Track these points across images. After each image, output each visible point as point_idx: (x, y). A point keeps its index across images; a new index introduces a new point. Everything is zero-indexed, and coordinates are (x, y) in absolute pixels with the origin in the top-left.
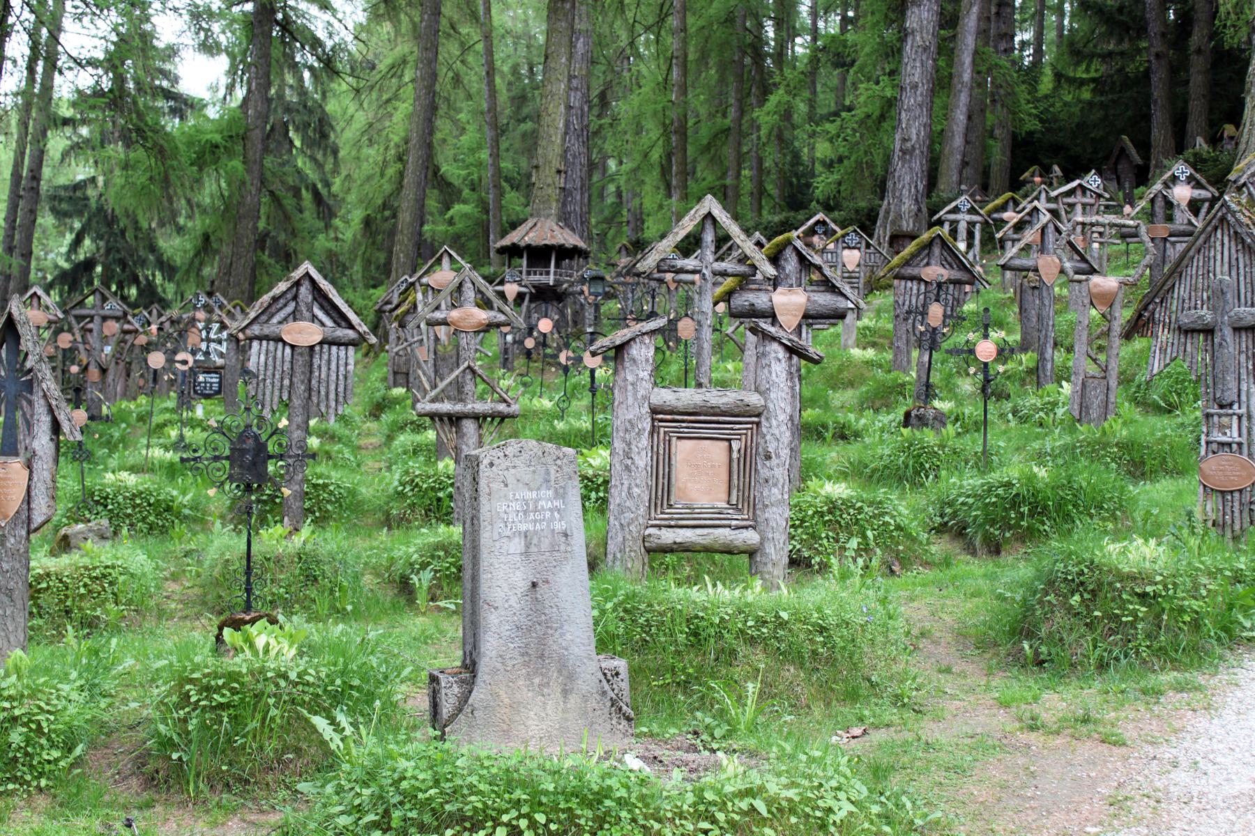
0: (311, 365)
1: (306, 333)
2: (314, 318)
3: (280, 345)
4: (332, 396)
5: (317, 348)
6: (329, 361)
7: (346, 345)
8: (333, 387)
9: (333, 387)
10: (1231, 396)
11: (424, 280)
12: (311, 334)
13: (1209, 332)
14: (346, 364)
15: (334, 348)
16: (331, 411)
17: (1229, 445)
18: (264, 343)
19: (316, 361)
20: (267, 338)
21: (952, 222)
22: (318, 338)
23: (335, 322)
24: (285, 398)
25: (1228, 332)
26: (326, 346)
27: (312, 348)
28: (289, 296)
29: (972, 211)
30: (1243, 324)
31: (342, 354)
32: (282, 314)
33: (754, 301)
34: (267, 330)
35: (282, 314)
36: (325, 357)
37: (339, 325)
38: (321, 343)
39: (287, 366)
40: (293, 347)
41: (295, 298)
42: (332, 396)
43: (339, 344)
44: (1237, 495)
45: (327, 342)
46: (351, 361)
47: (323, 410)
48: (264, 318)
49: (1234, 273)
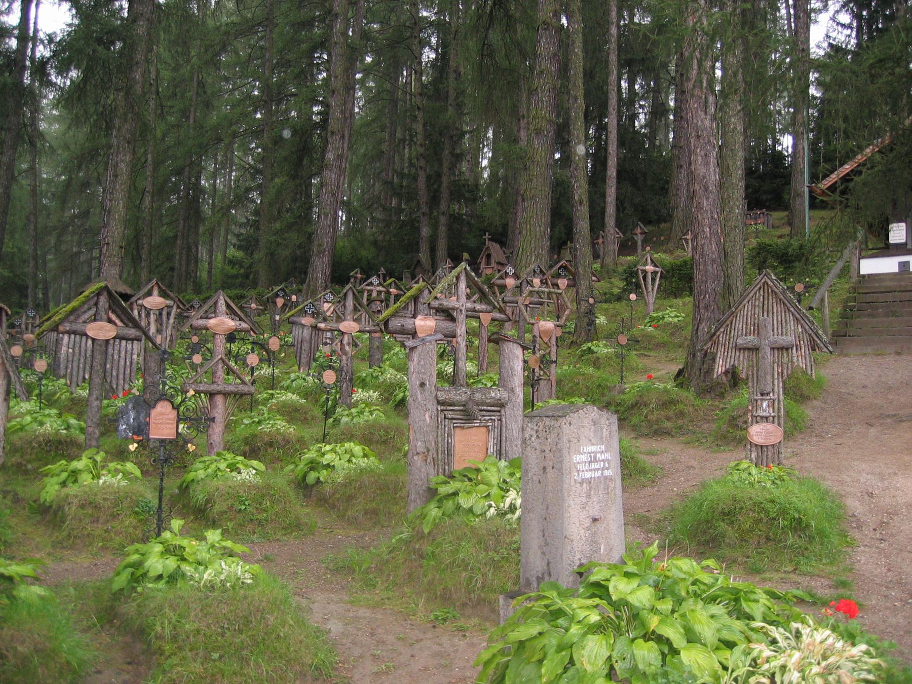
0: (106, 354)
1: (102, 330)
2: (110, 321)
3: (84, 338)
4: (121, 376)
5: (111, 342)
6: (120, 352)
7: (132, 340)
8: (122, 371)
9: (122, 371)
10: (769, 389)
11: (140, 302)
12: (109, 331)
13: (755, 349)
14: (132, 354)
15: (124, 342)
16: (120, 388)
17: (767, 418)
18: (73, 336)
19: (110, 350)
20: (75, 333)
21: (369, 291)
22: (113, 334)
23: (124, 323)
24: (87, 376)
25: (768, 350)
26: (118, 340)
27: (107, 341)
28: (92, 302)
29: (380, 284)
30: (777, 345)
31: (129, 347)
32: (86, 316)
33: (404, 323)
34: (77, 327)
35: (86, 316)
36: (117, 348)
37: (127, 326)
38: (114, 338)
39: (89, 353)
40: (93, 340)
41: (96, 304)
42: (121, 376)
43: (127, 340)
44: (770, 448)
45: (119, 337)
46: (135, 351)
47: (115, 386)
48: (72, 318)
49: (770, 315)
